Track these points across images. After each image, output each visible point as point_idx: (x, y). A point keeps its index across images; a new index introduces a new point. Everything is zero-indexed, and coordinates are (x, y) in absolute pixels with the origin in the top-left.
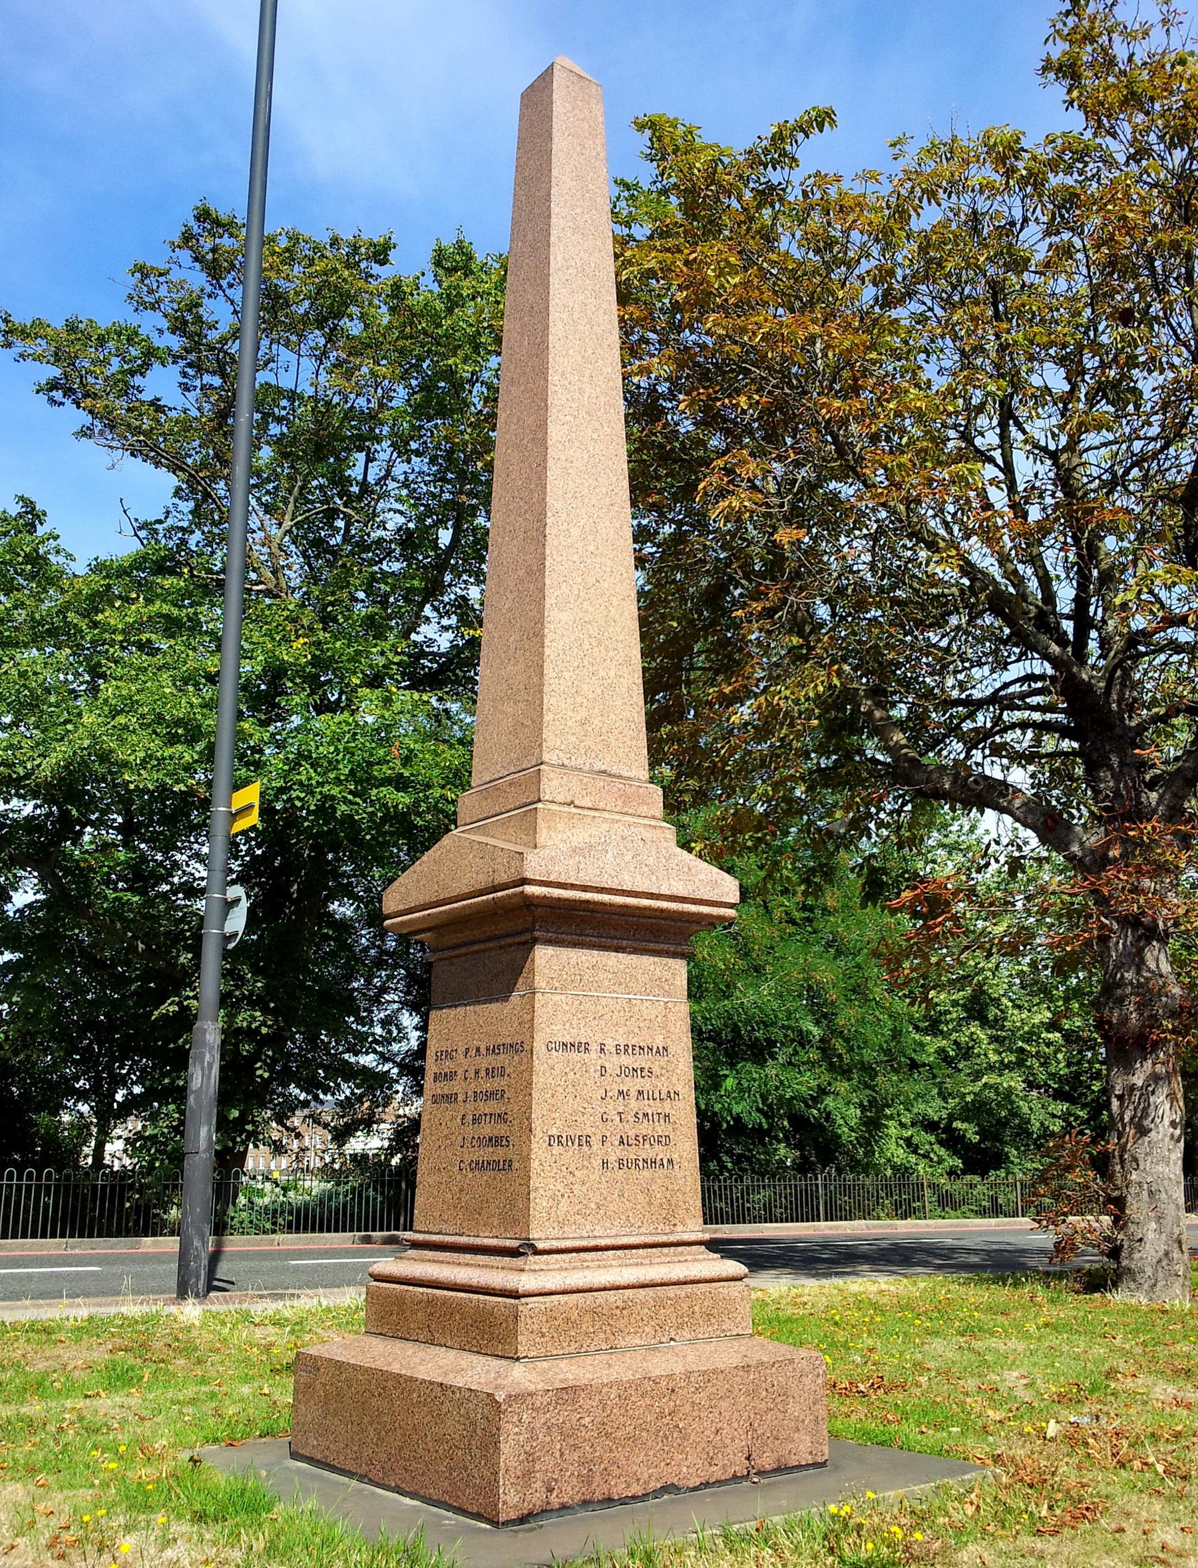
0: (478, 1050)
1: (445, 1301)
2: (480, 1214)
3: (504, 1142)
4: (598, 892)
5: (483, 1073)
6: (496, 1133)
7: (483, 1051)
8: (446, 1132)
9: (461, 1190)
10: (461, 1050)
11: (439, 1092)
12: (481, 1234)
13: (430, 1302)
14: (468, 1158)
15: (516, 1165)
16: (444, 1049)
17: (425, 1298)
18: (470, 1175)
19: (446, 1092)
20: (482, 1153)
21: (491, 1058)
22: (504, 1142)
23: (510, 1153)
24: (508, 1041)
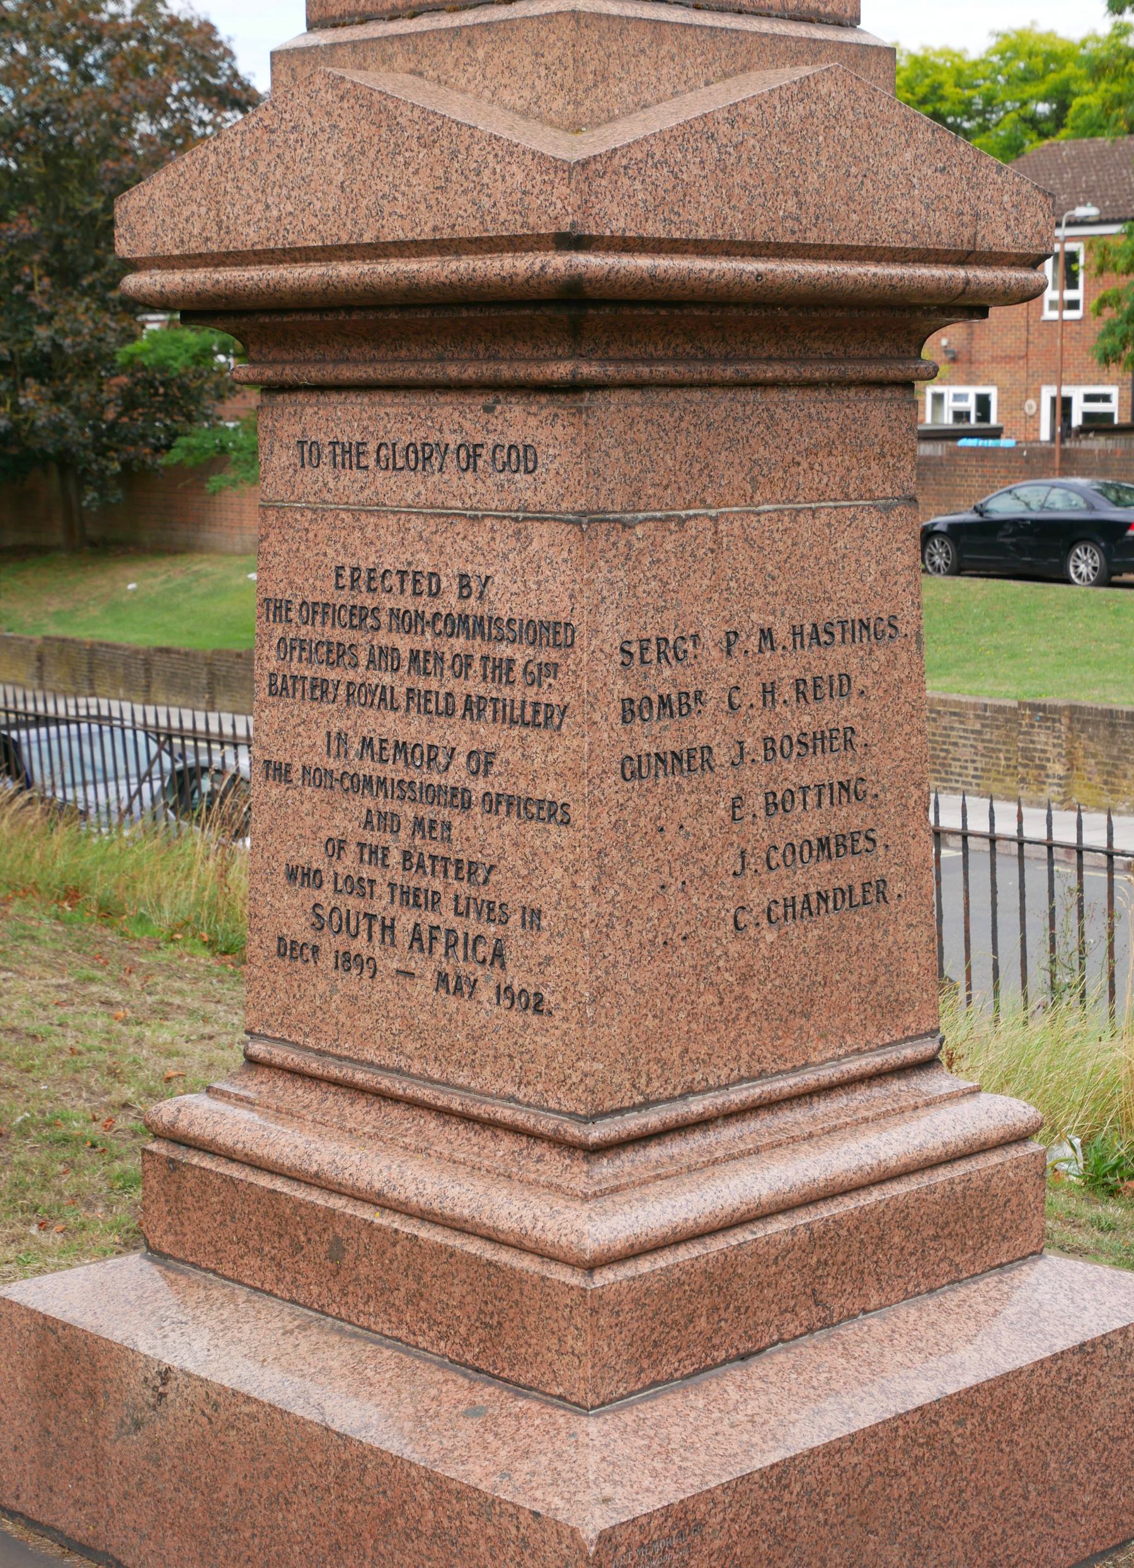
0: (766, 634)
1: (863, 1216)
2: (806, 1016)
3: (862, 844)
4: (728, 254)
5: (787, 692)
6: (835, 827)
7: (782, 633)
8: (680, 845)
9: (744, 979)
10: (713, 634)
11: (646, 746)
12: (815, 1058)
13: (817, 1239)
14: (757, 898)
15: (896, 887)
16: (651, 633)
17: (803, 1235)
18: (770, 937)
19: (669, 745)
20: (800, 878)
21: (811, 654)
22: (862, 844)
23: (881, 865)
24: (855, 613)
